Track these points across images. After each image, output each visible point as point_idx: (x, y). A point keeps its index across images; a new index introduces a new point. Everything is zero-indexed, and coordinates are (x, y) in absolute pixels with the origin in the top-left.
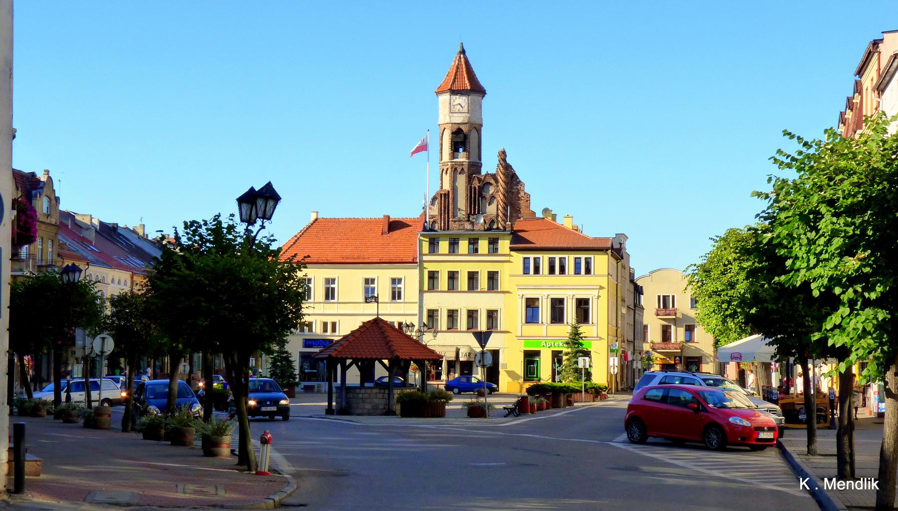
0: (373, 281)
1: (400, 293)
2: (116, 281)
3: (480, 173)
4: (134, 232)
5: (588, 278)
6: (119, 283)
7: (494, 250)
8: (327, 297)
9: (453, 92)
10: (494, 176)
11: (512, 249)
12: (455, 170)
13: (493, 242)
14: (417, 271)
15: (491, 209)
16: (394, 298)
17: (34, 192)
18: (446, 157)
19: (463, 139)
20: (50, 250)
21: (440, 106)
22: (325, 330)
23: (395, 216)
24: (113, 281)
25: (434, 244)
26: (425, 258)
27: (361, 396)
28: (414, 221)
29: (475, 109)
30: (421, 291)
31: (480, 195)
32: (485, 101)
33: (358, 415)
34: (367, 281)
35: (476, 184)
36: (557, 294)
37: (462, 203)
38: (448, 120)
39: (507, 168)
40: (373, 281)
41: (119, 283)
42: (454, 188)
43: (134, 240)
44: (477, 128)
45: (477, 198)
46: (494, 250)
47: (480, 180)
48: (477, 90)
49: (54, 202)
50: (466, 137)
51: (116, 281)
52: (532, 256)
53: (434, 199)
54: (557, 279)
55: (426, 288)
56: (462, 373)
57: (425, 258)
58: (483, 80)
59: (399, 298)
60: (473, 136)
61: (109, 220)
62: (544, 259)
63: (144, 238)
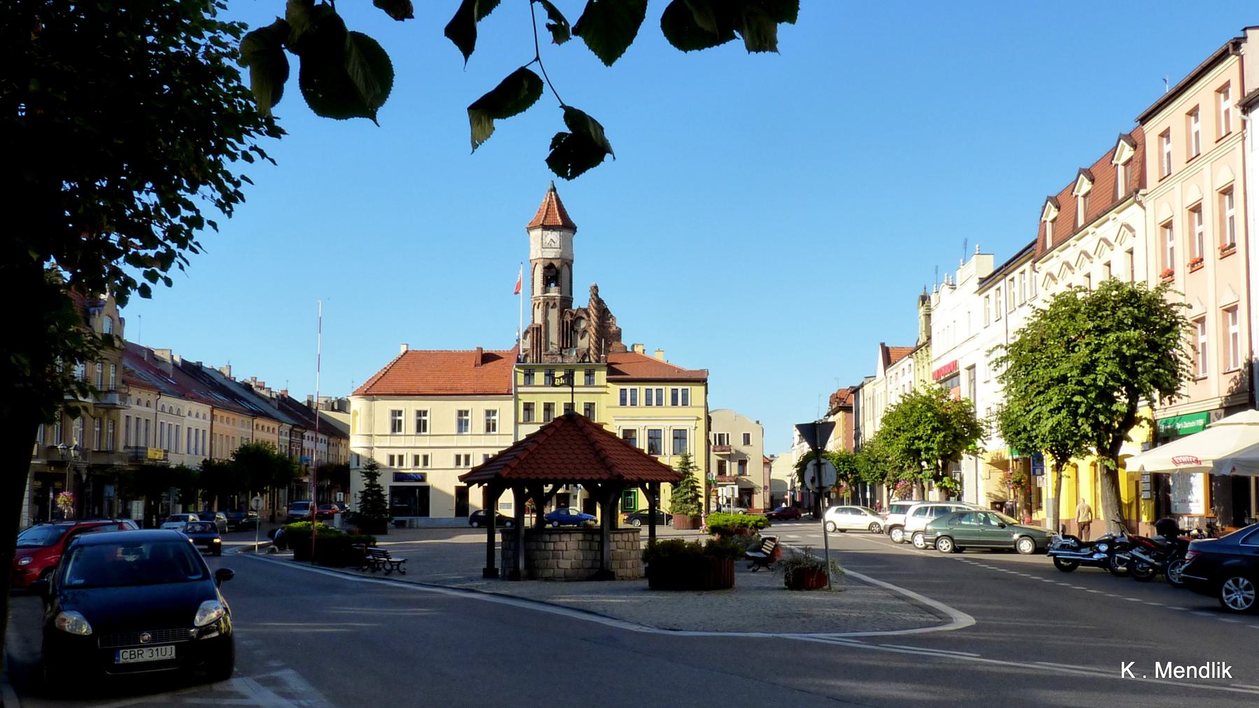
0: (466, 413)
1: (494, 425)
2: (194, 414)
3: (570, 307)
4: (220, 372)
5: (685, 409)
6: (197, 416)
7: (590, 382)
8: (419, 430)
9: (545, 227)
10: (585, 311)
11: (608, 381)
12: (547, 305)
13: (589, 374)
14: (512, 403)
15: (583, 343)
16: (488, 430)
17: (92, 310)
18: (538, 291)
19: (555, 274)
20: (113, 375)
21: (532, 242)
22: (417, 463)
23: (487, 349)
24: (190, 414)
25: (529, 375)
26: (520, 390)
27: (551, 546)
28: (508, 353)
29: (566, 245)
30: (517, 423)
31: (572, 328)
32: (576, 238)
33: (547, 579)
34: (461, 413)
35: (568, 318)
36: (654, 425)
37: (554, 337)
38: (540, 256)
39: (599, 302)
40: (466, 413)
41: (197, 416)
42: (546, 322)
43: (219, 379)
44: (568, 263)
45: (569, 331)
46: (590, 382)
47: (572, 315)
48: (568, 226)
49: (117, 323)
50: (558, 272)
51: (194, 414)
52: (628, 387)
53: (526, 332)
54: (654, 411)
55: (521, 419)
56: (558, 506)
57: (520, 390)
58: (574, 218)
59: (494, 430)
60: (565, 271)
61: (192, 360)
62: (641, 389)
63: (234, 381)
